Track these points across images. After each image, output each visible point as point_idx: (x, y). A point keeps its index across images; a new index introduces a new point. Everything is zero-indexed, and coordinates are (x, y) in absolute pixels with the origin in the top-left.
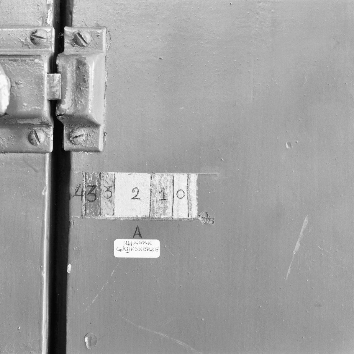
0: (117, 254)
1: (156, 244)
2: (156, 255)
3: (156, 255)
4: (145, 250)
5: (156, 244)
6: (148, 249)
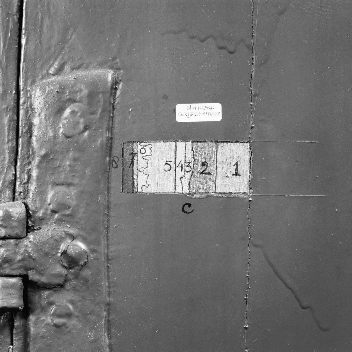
2: (218, 118)
3: (218, 118)
6: (186, 113)
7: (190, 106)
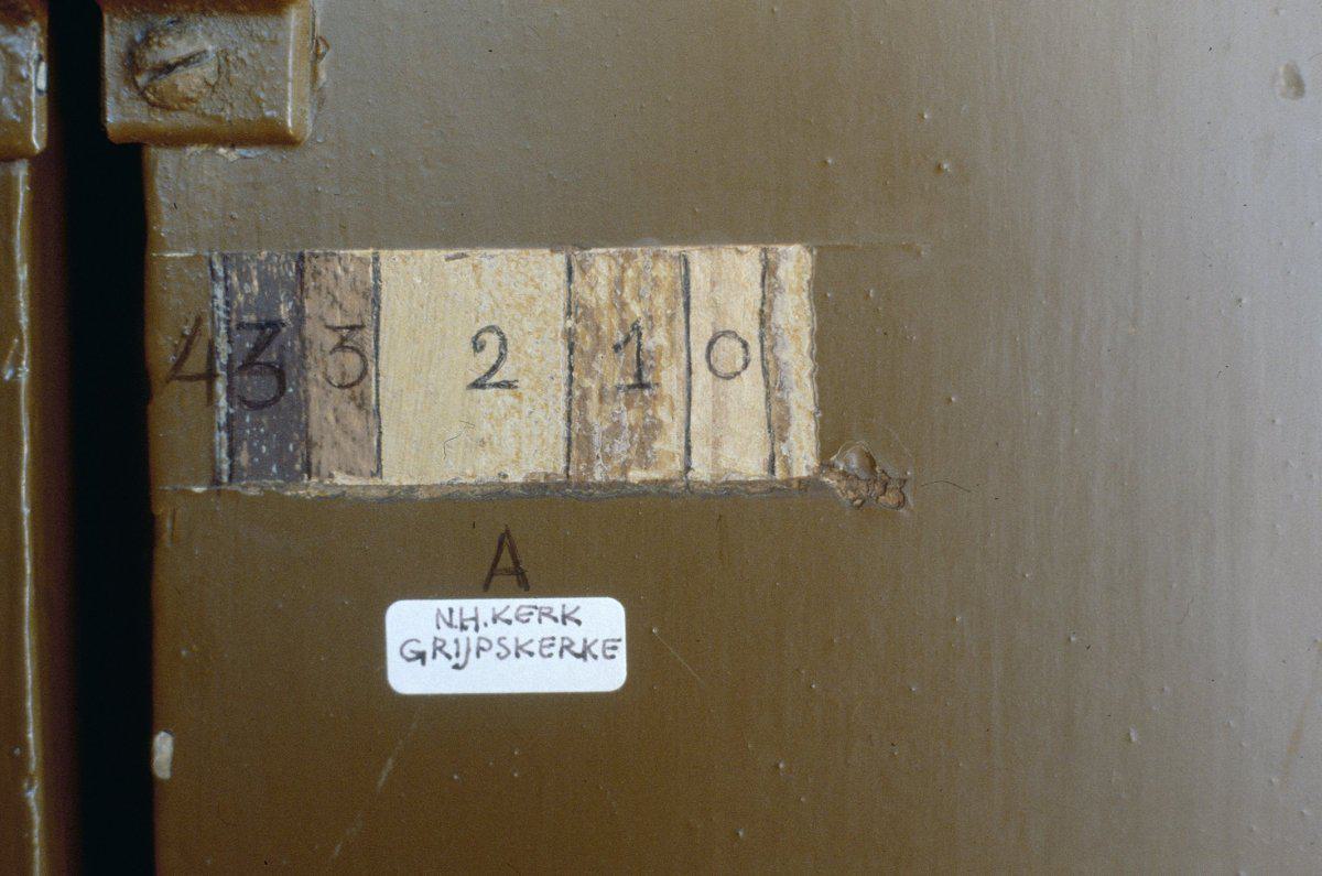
0: (405, 679)
1: (604, 617)
2: (608, 675)
4: (550, 655)
5: (604, 617)
7: (451, 611)
